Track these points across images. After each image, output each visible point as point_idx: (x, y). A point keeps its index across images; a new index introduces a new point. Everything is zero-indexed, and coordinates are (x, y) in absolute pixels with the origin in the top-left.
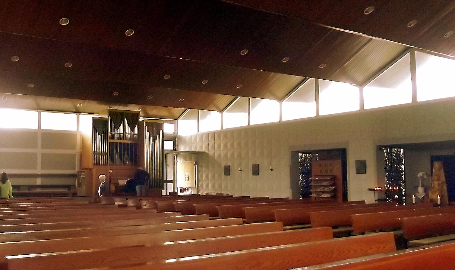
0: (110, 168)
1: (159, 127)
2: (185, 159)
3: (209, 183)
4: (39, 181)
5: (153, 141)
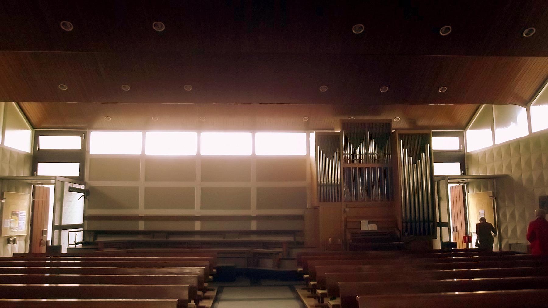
0: (347, 205)
1: (426, 140)
2: (479, 188)
3: (516, 226)
4: (254, 226)
5: (415, 162)
